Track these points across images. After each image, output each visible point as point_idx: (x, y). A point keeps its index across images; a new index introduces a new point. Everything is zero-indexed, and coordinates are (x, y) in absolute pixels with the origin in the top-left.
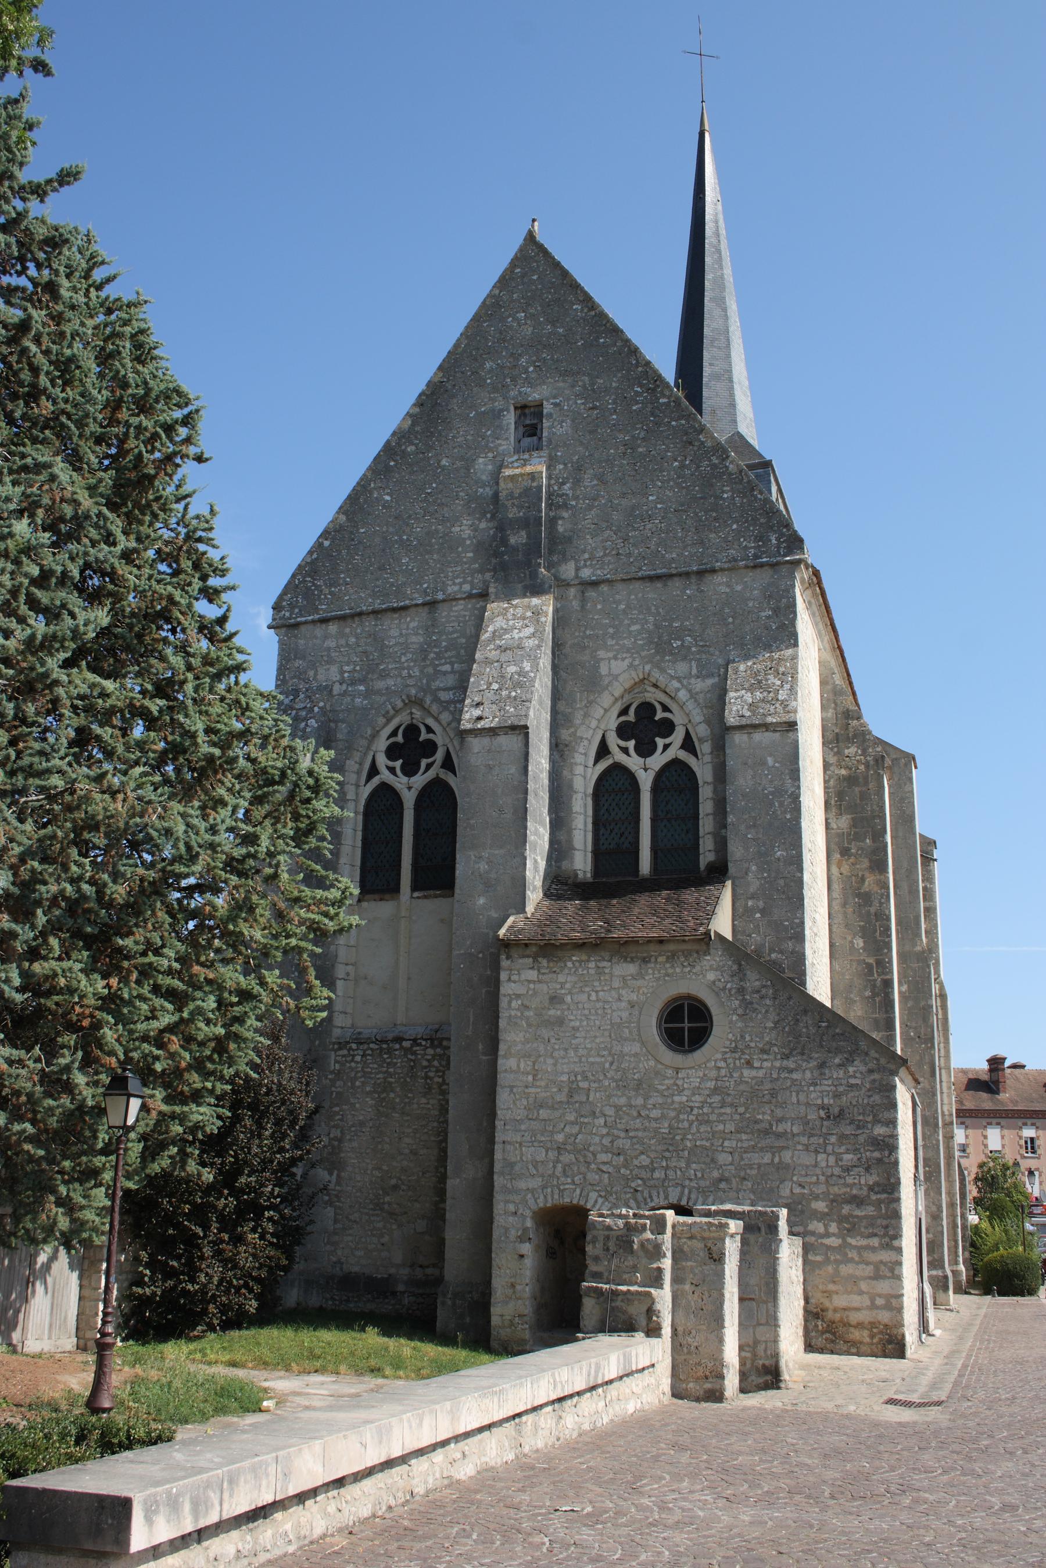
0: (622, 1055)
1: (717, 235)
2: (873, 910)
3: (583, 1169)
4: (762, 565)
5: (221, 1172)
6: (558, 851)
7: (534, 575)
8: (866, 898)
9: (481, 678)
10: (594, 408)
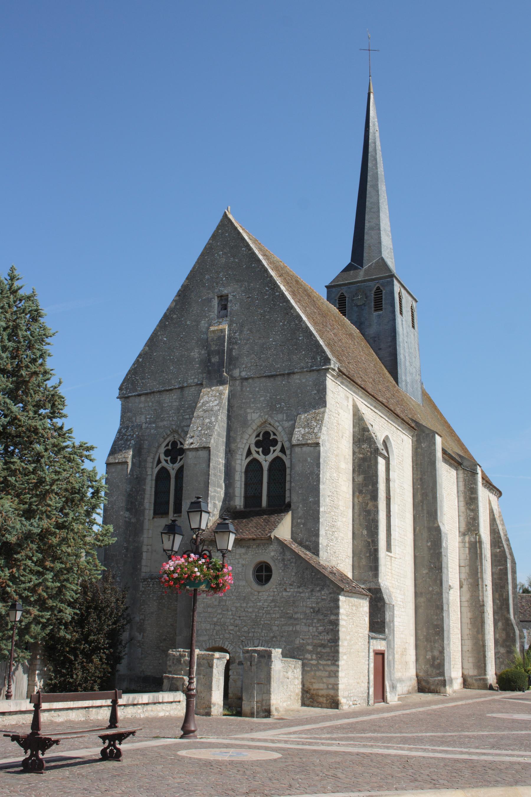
1: (375, 150)
2: (371, 518)
3: (223, 632)
4: (313, 370)
6: (228, 496)
7: (221, 376)
8: (368, 512)
9: (195, 427)
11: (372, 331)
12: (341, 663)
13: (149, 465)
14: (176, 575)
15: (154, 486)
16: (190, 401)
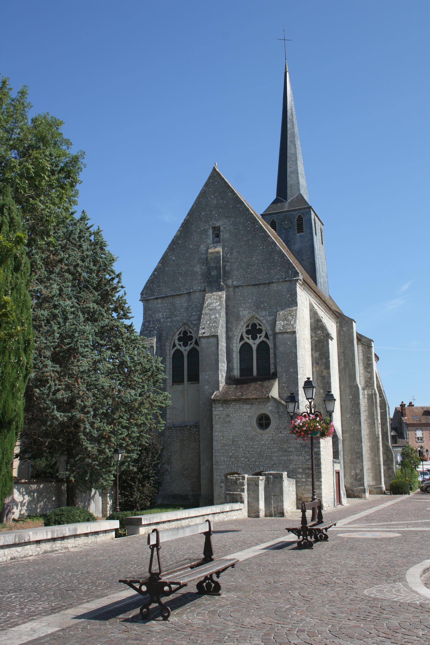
0: (247, 431)
1: (292, 115)
2: (326, 381)
3: (237, 463)
5: (138, 468)
6: (229, 369)
7: (219, 284)
8: (323, 378)
9: (204, 320)
10: (236, 229)
11: (296, 247)
12: (323, 480)
13: (168, 348)
14: (305, 428)
15: (171, 363)
16: (196, 302)
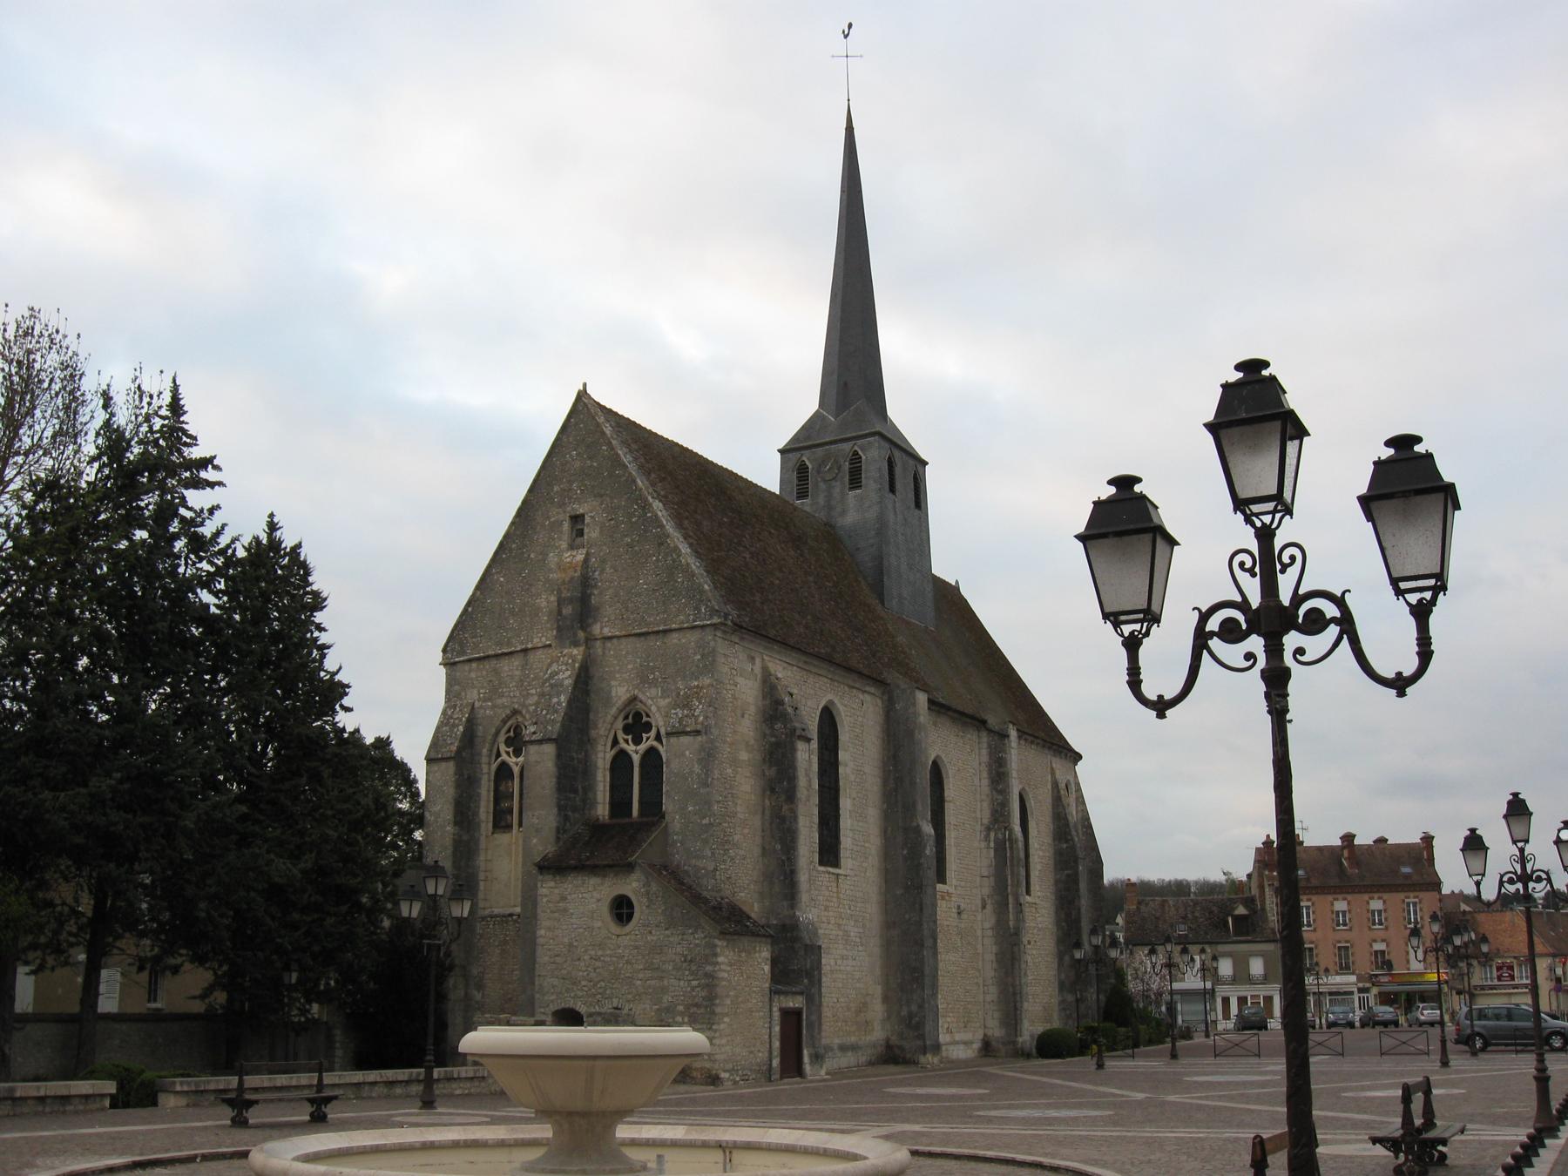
13: (484, 760)
